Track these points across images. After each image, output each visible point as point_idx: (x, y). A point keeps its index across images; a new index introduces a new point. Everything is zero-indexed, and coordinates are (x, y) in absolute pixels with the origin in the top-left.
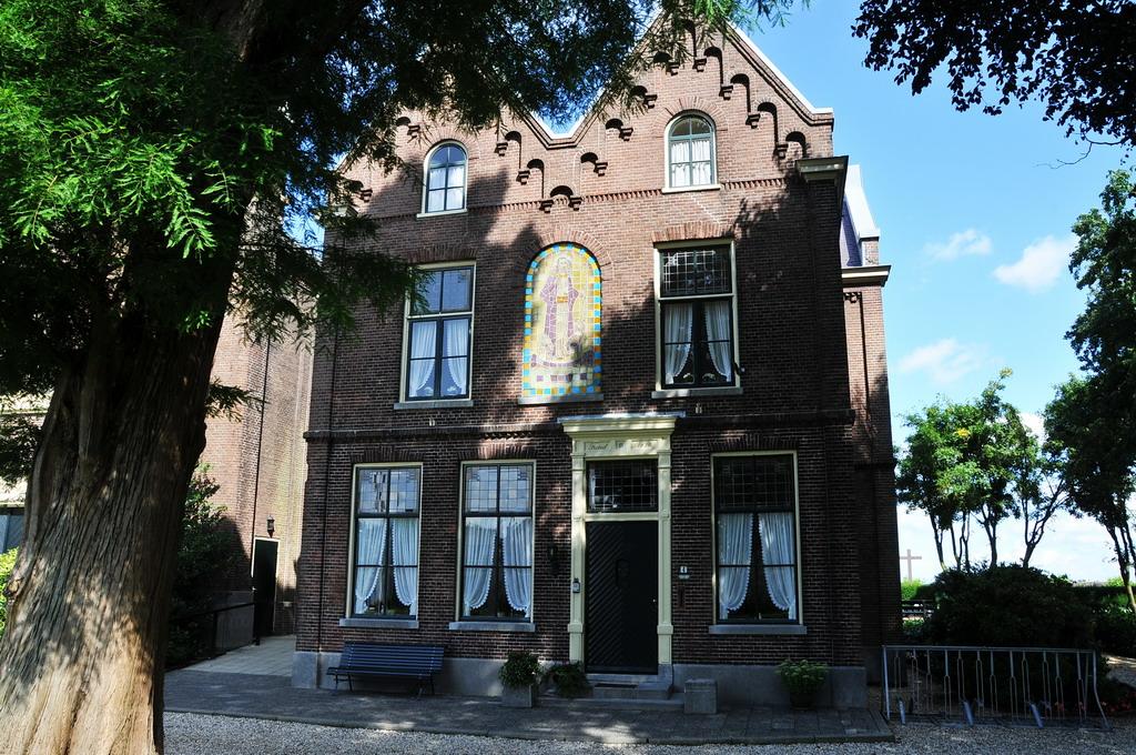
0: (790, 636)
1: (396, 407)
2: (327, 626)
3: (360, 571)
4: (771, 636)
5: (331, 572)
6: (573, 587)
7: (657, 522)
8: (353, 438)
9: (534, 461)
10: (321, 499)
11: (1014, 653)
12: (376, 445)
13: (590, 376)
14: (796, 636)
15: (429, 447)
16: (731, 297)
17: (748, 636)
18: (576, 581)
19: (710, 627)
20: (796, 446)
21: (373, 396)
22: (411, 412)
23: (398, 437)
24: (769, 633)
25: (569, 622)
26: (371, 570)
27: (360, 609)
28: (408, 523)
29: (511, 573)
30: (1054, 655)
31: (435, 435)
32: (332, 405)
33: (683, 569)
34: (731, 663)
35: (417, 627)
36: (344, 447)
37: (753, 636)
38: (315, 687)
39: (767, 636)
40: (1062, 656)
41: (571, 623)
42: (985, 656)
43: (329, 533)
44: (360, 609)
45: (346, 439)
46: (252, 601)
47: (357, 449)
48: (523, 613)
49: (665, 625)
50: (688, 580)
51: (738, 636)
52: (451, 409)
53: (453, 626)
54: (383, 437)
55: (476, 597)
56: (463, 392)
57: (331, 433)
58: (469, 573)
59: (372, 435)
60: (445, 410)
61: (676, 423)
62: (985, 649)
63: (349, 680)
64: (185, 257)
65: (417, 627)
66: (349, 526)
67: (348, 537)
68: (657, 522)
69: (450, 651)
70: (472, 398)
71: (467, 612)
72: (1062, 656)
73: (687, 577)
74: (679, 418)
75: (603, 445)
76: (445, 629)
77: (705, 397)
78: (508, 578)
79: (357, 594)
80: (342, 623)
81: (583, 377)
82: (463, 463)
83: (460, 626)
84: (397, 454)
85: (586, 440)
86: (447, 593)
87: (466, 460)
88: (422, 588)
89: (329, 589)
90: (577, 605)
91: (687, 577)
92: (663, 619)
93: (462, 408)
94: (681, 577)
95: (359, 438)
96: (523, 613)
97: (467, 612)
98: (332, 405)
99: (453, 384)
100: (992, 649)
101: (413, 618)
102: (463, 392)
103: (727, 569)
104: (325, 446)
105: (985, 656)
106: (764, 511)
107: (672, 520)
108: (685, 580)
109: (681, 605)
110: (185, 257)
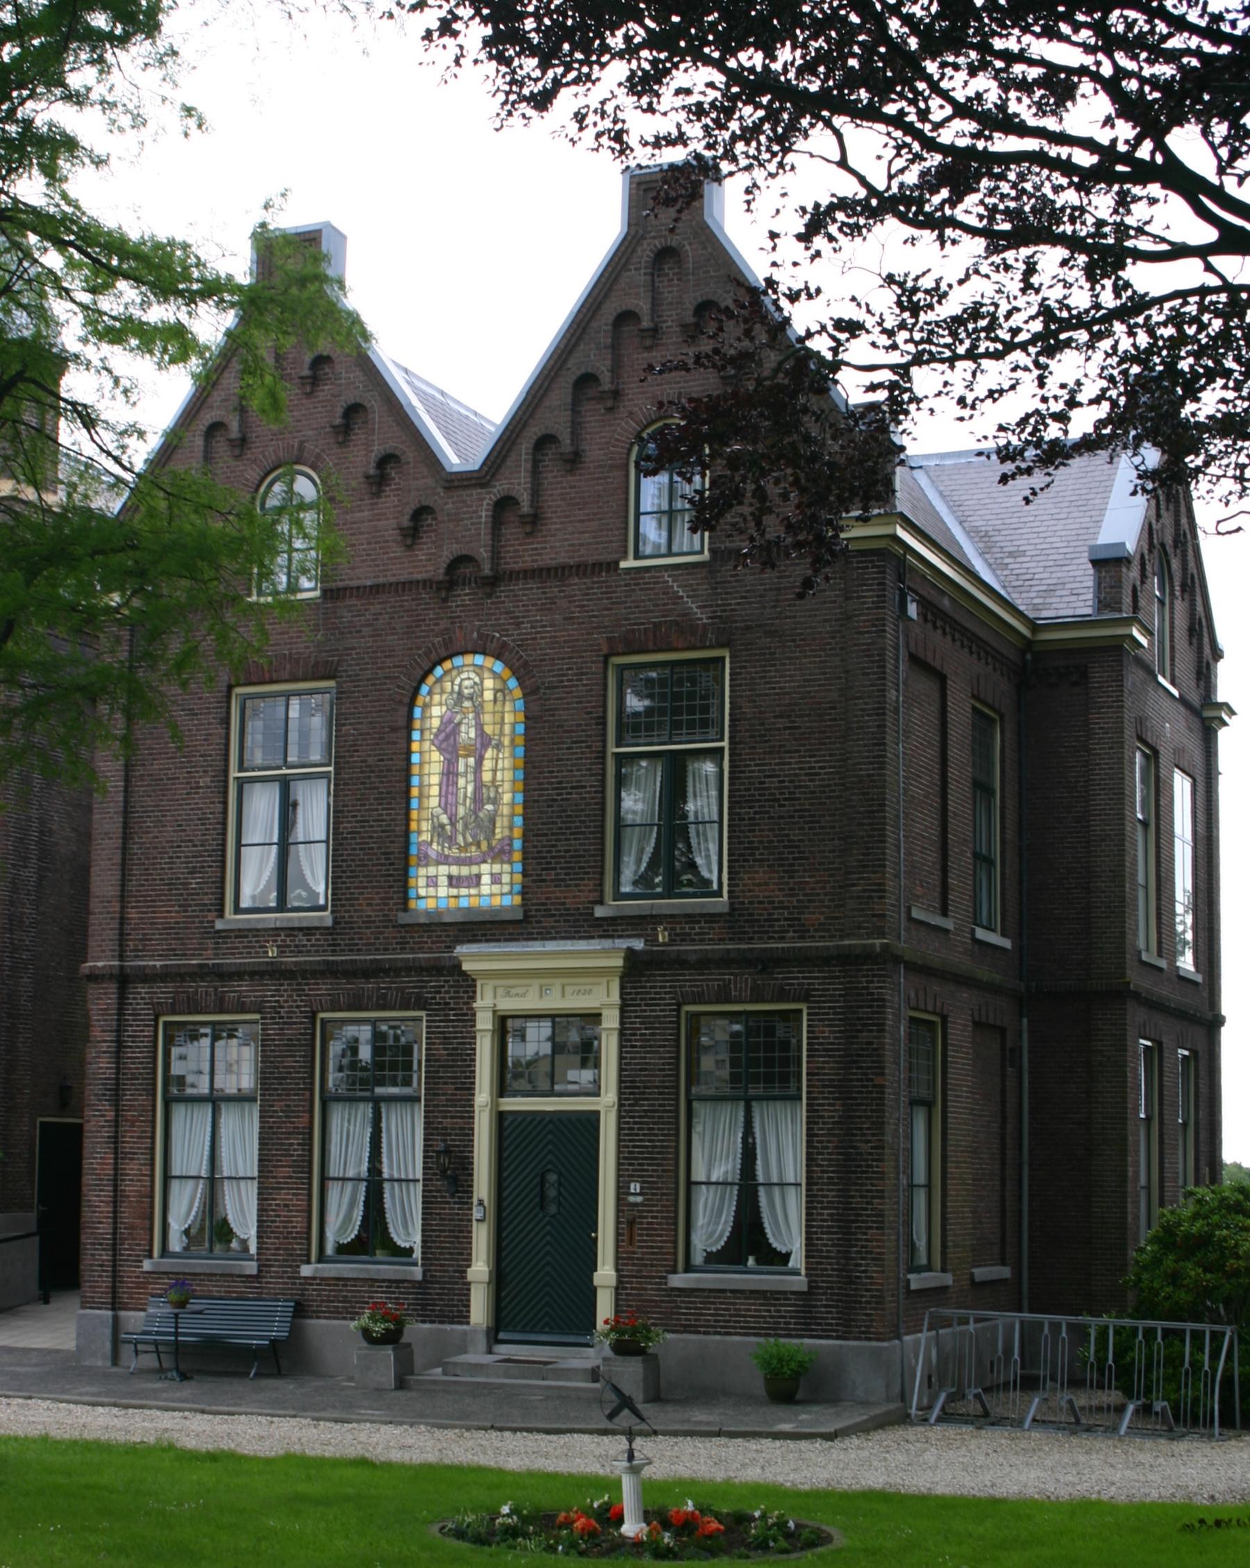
0: (785, 1293)
1: (219, 925)
2: (126, 1269)
3: (175, 1185)
4: (757, 1292)
5: (131, 1188)
6: (477, 1213)
7: (597, 1113)
8: (156, 975)
9: (423, 1014)
10: (110, 1073)
11: (1163, 1329)
12: (190, 987)
13: (506, 878)
14: (793, 1293)
15: (268, 992)
16: (722, 749)
17: (724, 1291)
18: (481, 1203)
19: (671, 1276)
20: (805, 997)
21: (185, 907)
22: (241, 933)
23: (223, 975)
24: (753, 1288)
25: (469, 1266)
26: (191, 1183)
27: (176, 1244)
28: (243, 1110)
29: (393, 1188)
30: (1059, 1325)
31: (276, 973)
32: (123, 920)
33: (635, 1187)
34: (699, 1332)
35: (255, 1272)
36: (143, 990)
37: (732, 1291)
38: (109, 1363)
39: (752, 1292)
40: (1071, 1326)
41: (473, 1268)
42: (1055, 1327)
43: (125, 1127)
44: (176, 1244)
45: (148, 977)
46: (34, 1229)
47: (163, 992)
48: (786, 1257)
49: (605, 1274)
50: (642, 1204)
51: (710, 1290)
52: (300, 929)
53: (306, 1271)
54: (202, 973)
55: (344, 1227)
56: (322, 902)
57: (122, 967)
58: (334, 1191)
59: (182, 970)
60: (291, 931)
61: (626, 959)
62: (1150, 1323)
63: (158, 1352)
64: (1201, 197)
65: (255, 1272)
66: (154, 1116)
67: (154, 1132)
68: (597, 1113)
69: (301, 1310)
70: (332, 912)
71: (330, 1249)
72: (1071, 1326)
73: (639, 1199)
74: (630, 952)
75: (520, 990)
76: (295, 1275)
77: (672, 916)
78: (390, 1195)
79: (171, 1220)
80: (147, 1265)
81: (496, 879)
82: (322, 1015)
83: (316, 1270)
84: (222, 999)
85: (565, 981)
86: (298, 1221)
87: (323, 1011)
88: (262, 1210)
89: (127, 1215)
90: (481, 1239)
91: (639, 1199)
92: (604, 1264)
93: (317, 928)
94: (632, 1199)
95: (164, 976)
96: (786, 1257)
97: (330, 1249)
98: (123, 920)
99: (306, 887)
100: (1159, 1325)
101: (796, 1273)
102: (322, 902)
103: (704, 1187)
104: (113, 988)
105: (1055, 1327)
106: (759, 1099)
107: (619, 1111)
108: (636, 1204)
109: (631, 1242)
110: (1201, 197)
